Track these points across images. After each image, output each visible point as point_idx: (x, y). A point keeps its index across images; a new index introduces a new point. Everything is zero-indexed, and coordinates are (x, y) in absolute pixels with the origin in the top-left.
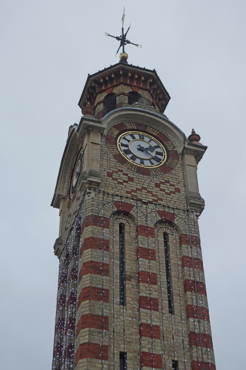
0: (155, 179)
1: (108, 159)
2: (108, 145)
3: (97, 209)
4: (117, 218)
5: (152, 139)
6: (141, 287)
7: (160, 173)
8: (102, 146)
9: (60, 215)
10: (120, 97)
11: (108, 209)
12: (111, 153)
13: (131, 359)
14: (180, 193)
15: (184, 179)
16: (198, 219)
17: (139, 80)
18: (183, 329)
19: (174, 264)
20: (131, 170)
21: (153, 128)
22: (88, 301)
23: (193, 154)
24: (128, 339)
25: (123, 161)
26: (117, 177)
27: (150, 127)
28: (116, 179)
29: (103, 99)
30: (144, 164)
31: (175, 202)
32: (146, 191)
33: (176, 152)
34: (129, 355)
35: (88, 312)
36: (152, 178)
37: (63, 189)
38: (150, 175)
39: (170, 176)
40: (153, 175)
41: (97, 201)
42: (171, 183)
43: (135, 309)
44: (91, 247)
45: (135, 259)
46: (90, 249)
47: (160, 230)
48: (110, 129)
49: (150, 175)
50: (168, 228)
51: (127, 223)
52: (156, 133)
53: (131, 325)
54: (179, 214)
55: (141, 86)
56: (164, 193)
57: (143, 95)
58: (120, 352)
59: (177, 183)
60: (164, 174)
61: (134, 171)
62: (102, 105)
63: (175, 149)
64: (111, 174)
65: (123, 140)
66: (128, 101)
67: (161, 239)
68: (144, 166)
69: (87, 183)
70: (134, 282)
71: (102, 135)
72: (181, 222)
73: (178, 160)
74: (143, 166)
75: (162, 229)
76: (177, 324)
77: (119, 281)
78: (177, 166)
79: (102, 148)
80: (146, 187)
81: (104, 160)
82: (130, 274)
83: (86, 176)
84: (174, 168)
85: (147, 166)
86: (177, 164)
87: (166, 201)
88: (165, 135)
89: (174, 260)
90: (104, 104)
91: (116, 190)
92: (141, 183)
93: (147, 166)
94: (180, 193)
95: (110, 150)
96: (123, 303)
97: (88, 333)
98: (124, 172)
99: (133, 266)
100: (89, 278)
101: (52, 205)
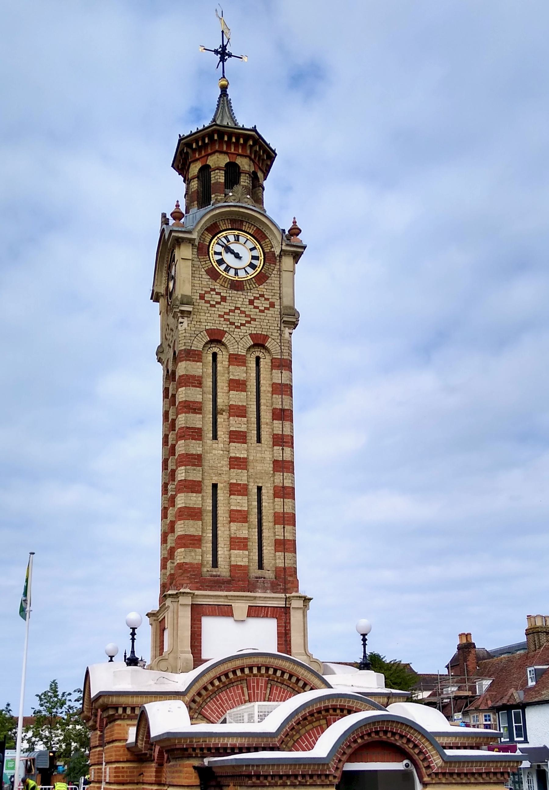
0: (249, 294)
1: (200, 276)
2: (199, 257)
3: (190, 341)
4: (211, 347)
5: (248, 238)
6: (231, 422)
7: (254, 286)
8: (194, 260)
9: (160, 314)
10: (215, 173)
11: (200, 340)
12: (203, 268)
13: (222, 489)
14: (274, 307)
15: (280, 290)
16: (10, 710)
17: (237, 144)
18: (268, 456)
19: (265, 391)
20: (224, 287)
21: (249, 223)
22: (184, 441)
23: (292, 255)
24: (219, 472)
25: (213, 274)
26: (209, 299)
27: (247, 222)
28: (208, 302)
29: (198, 173)
30: (238, 276)
31: (269, 320)
32: (239, 312)
33: (273, 253)
34: (220, 486)
35: (183, 452)
36: (246, 294)
37: (161, 285)
38: (244, 290)
39: (266, 287)
40: (248, 289)
41: (190, 332)
42: (266, 296)
43: (226, 443)
44: (186, 386)
45: (226, 391)
46: (184, 388)
47: (252, 354)
48: (202, 234)
49: (244, 290)
50: (260, 351)
51: (220, 351)
52: (253, 230)
53: (222, 458)
54: (272, 335)
55: (240, 151)
56: (258, 310)
57: (242, 165)
58: (213, 484)
59: (272, 296)
60: (259, 286)
61: (227, 288)
62: (196, 182)
63: (272, 250)
64: (203, 295)
65: (217, 245)
66: (224, 178)
67: (253, 365)
68: (238, 278)
69: (179, 312)
70: (225, 415)
71: (193, 245)
72: (273, 345)
73: (275, 264)
74: (237, 277)
75: (254, 353)
76: (263, 452)
77: (211, 416)
78: (274, 272)
79: (194, 262)
80: (239, 306)
81: (195, 279)
82: (222, 407)
83: (178, 303)
84: (269, 275)
85: (242, 278)
86: (273, 270)
87: (259, 320)
88: (262, 231)
89: (265, 387)
90: (198, 180)
91: (209, 315)
92: (234, 302)
93: (242, 278)
94: (274, 307)
95: (202, 263)
96: (215, 437)
97: (184, 471)
98: (217, 290)
99: (225, 398)
100: (183, 418)
101: (151, 299)
